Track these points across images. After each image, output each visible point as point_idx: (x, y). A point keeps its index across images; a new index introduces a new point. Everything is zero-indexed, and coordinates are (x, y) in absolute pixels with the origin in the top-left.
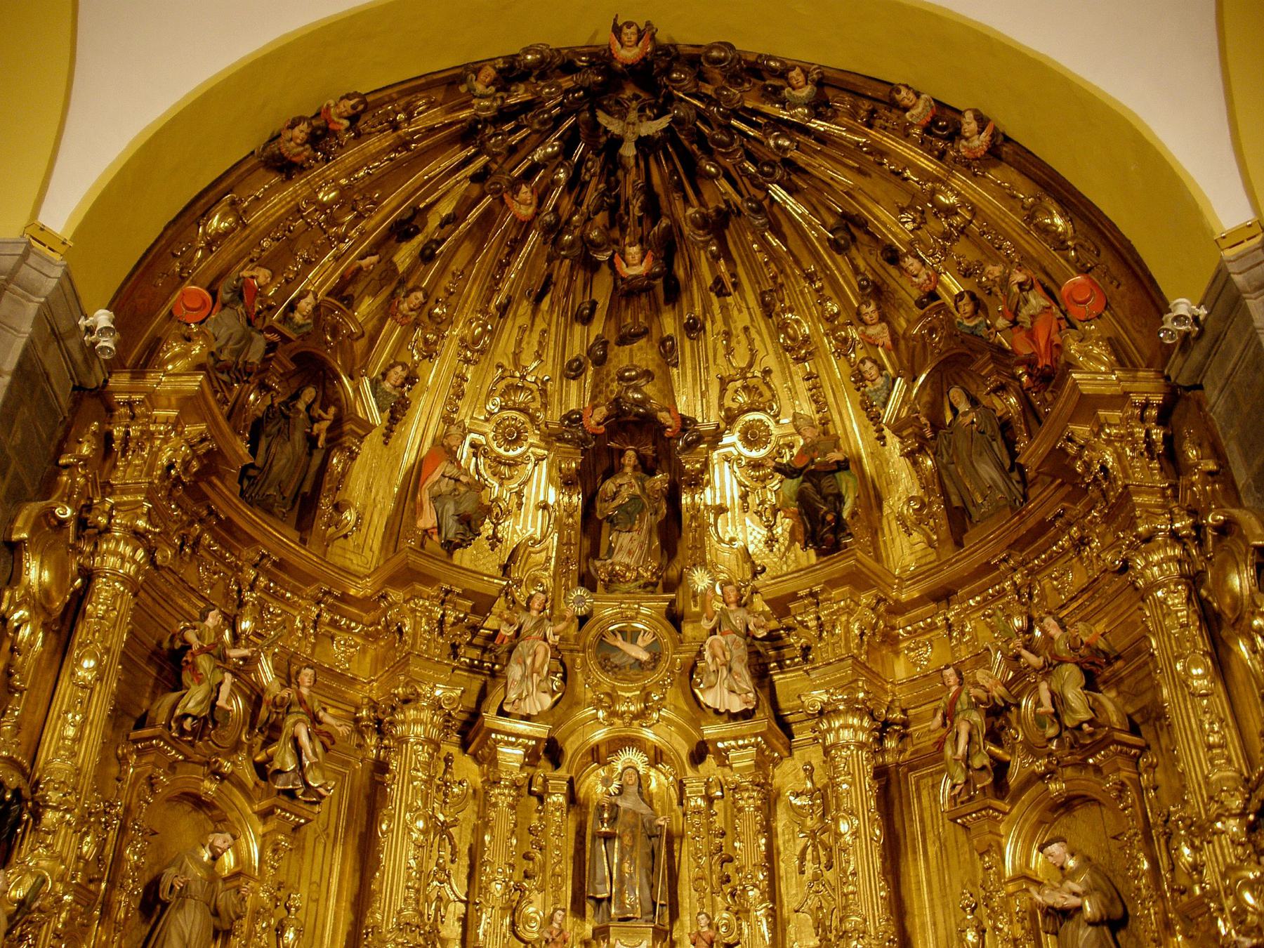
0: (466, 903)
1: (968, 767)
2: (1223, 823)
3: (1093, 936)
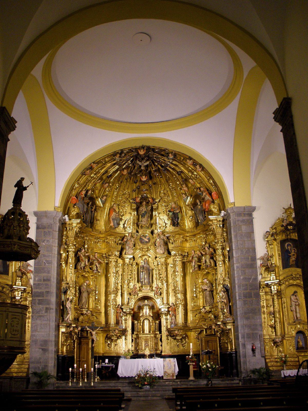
0: (121, 283)
1: (194, 266)
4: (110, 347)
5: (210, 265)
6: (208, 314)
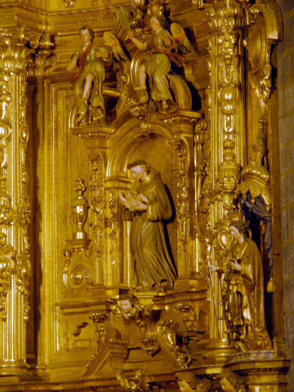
1: (89, 103)
2: (221, 196)
3: (151, 229)
5: (168, 101)
6: (145, 326)
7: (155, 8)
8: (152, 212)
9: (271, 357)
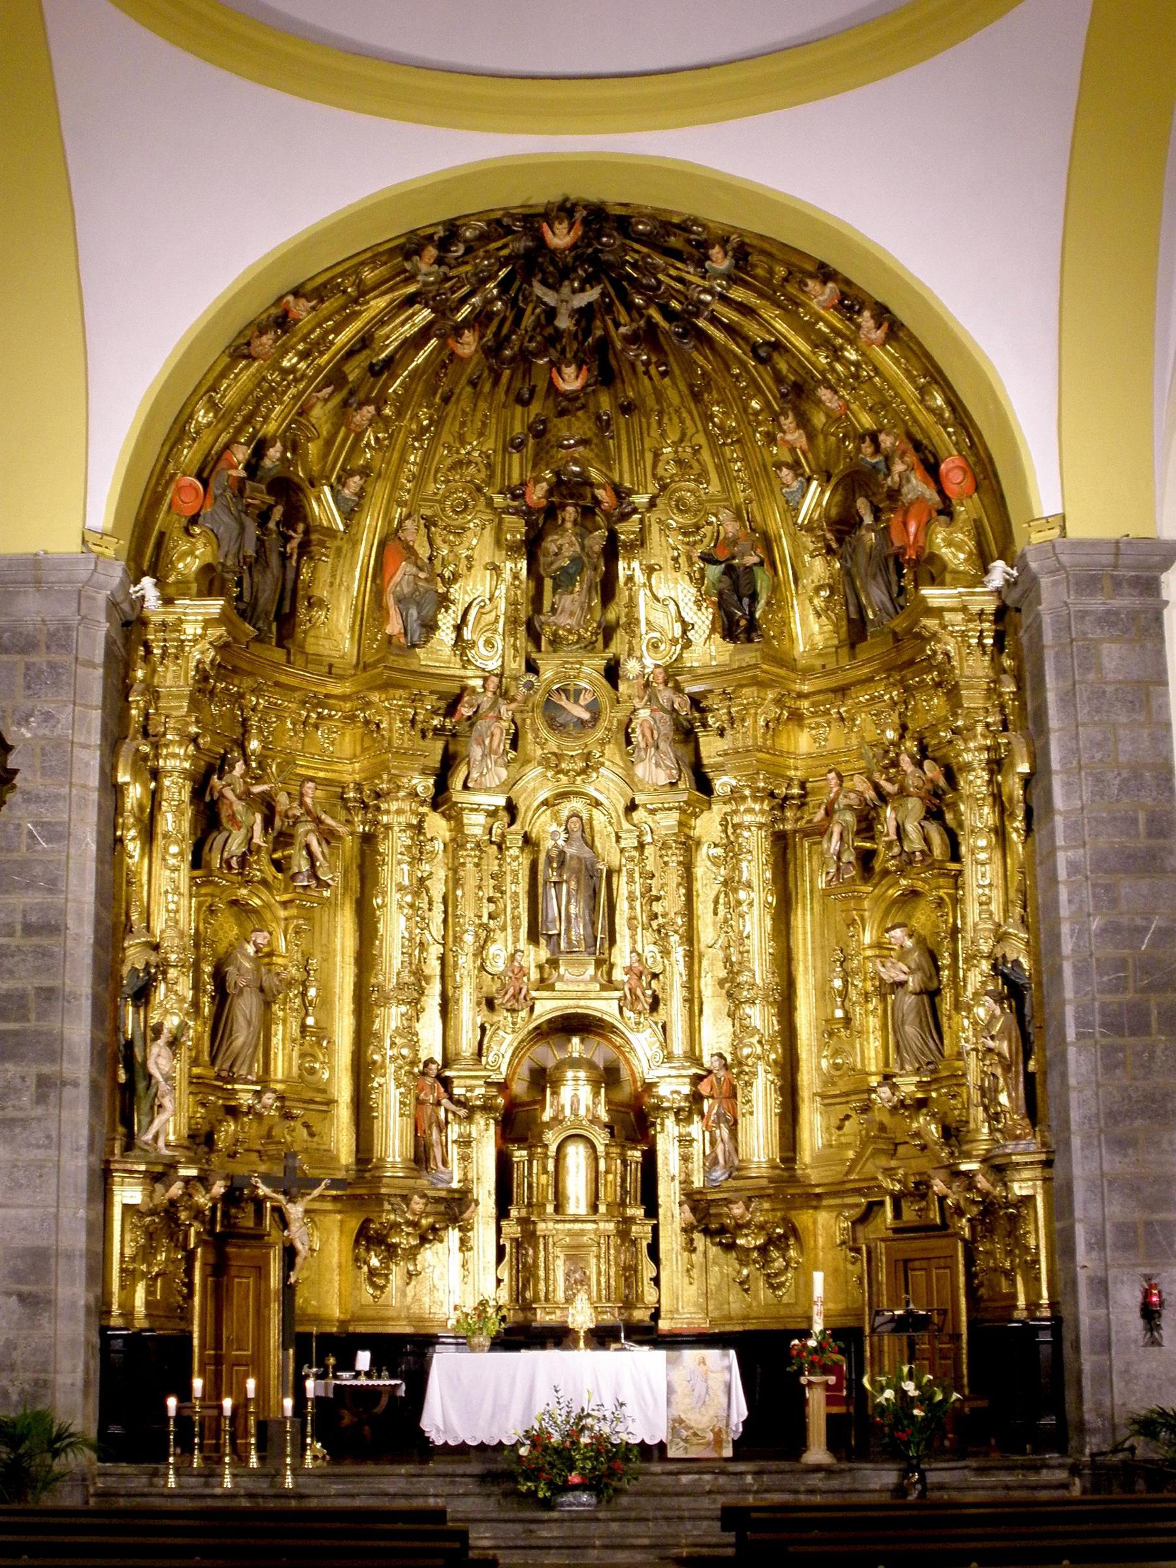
0: (444, 945)
1: (839, 859)
4: (382, 1288)
5: (922, 852)
6: (910, 1117)
7: (908, 744)
8: (913, 983)
9: (1032, 1148)
